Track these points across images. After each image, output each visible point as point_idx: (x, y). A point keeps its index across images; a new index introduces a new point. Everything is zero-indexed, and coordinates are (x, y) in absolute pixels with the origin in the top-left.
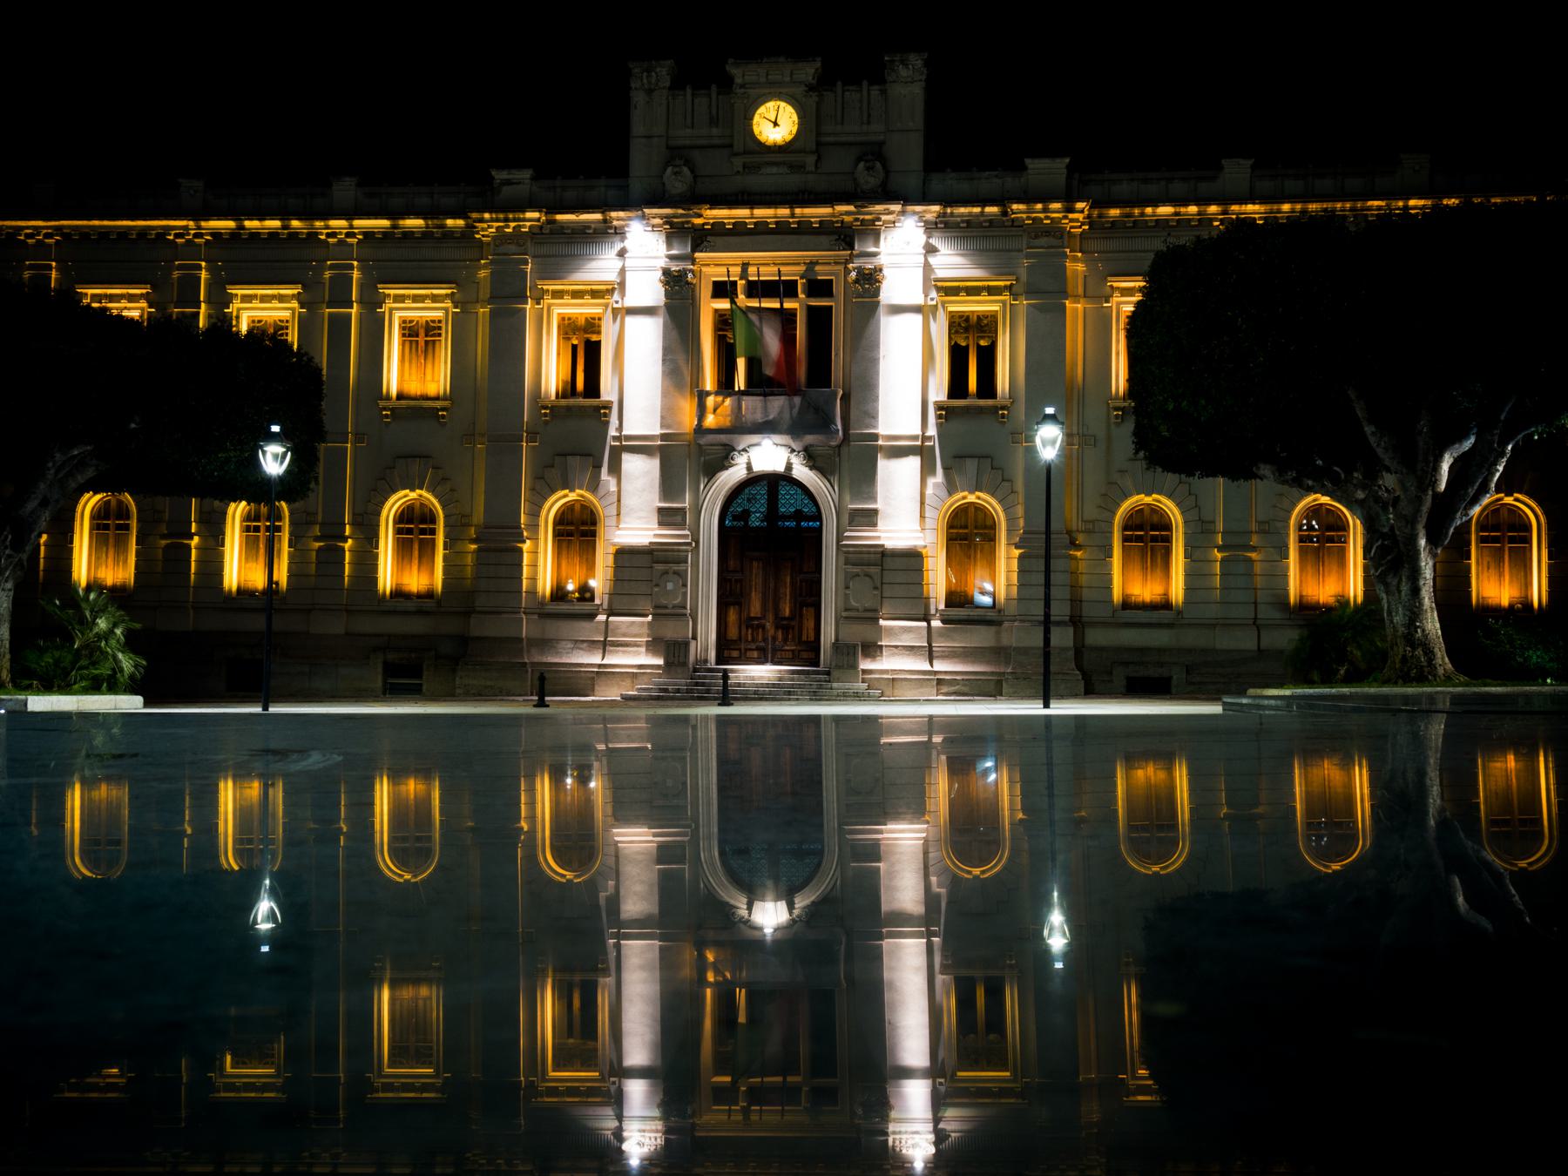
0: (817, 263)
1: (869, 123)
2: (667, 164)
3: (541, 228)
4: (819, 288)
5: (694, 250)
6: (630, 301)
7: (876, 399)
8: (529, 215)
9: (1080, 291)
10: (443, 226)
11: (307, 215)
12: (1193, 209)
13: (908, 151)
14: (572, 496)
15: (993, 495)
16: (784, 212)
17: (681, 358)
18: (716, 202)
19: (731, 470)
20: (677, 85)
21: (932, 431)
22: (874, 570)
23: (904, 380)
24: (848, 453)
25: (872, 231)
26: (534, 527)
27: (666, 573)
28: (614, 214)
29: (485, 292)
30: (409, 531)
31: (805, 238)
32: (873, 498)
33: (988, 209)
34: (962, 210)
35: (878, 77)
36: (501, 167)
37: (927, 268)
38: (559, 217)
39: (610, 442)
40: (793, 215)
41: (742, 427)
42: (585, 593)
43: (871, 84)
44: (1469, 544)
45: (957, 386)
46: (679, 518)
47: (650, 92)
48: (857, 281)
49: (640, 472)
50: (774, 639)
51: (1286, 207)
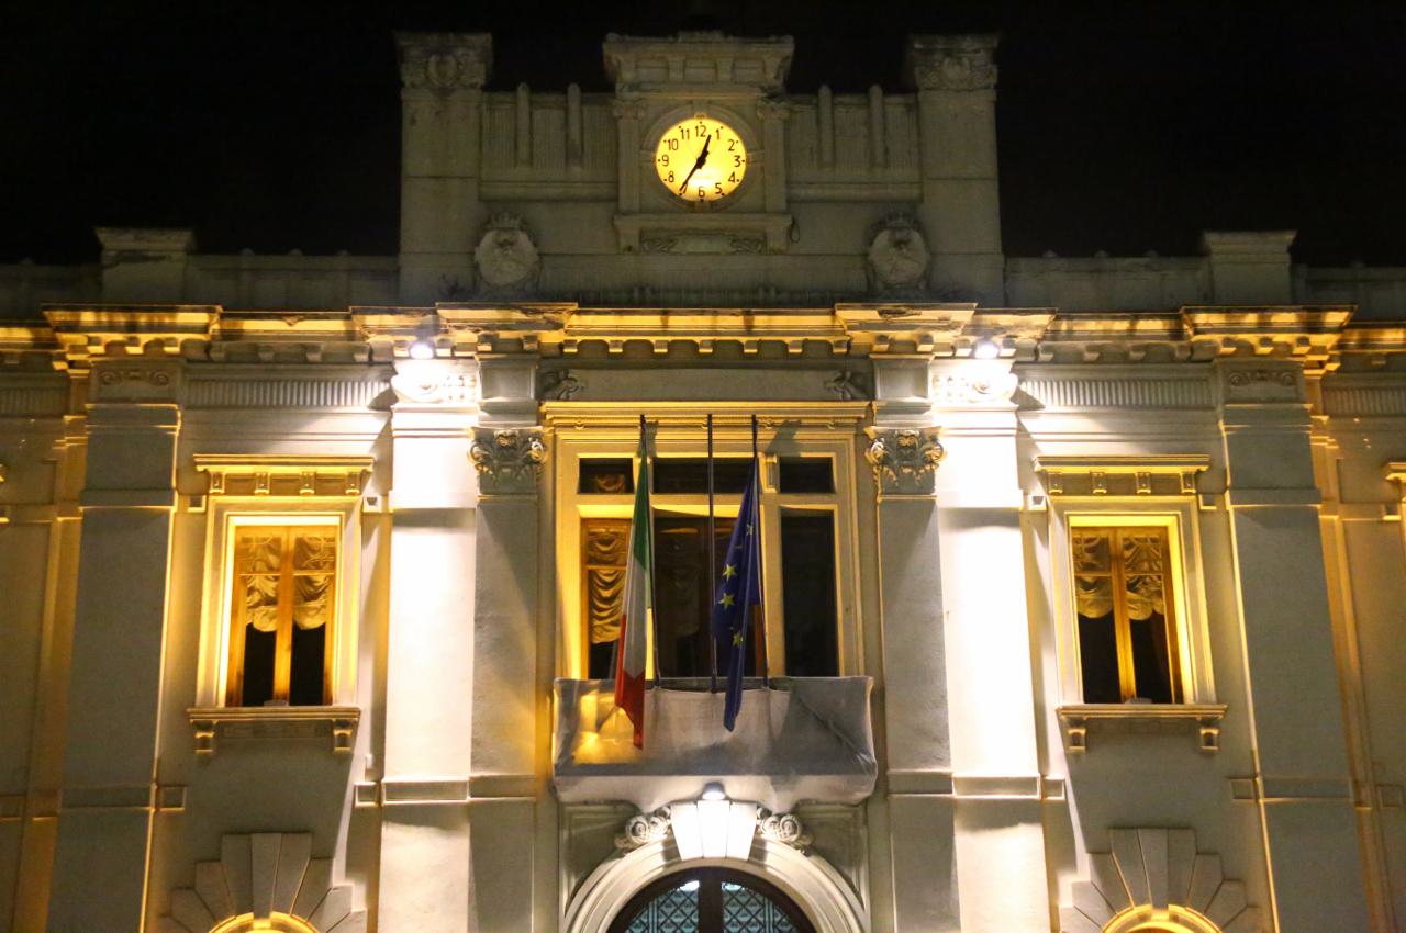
0: (799, 425)
1: (886, 165)
2: (484, 226)
3: (207, 347)
4: (805, 475)
5: (541, 396)
6: (405, 496)
7: (941, 701)
8: (184, 318)
9: (1334, 491)
13: (969, 210)
15: (1205, 911)
16: (731, 321)
17: (521, 620)
18: (591, 301)
19: (630, 858)
20: (500, 82)
21: (1059, 771)
23: (994, 677)
25: (911, 362)
28: (372, 320)
29: (73, 478)
31: (773, 376)
33: (1144, 325)
34: (1092, 326)
35: (899, 83)
36: (121, 222)
38: (250, 325)
39: (352, 801)
40: (749, 330)
45: (1099, 679)
47: (443, 92)
48: (884, 461)
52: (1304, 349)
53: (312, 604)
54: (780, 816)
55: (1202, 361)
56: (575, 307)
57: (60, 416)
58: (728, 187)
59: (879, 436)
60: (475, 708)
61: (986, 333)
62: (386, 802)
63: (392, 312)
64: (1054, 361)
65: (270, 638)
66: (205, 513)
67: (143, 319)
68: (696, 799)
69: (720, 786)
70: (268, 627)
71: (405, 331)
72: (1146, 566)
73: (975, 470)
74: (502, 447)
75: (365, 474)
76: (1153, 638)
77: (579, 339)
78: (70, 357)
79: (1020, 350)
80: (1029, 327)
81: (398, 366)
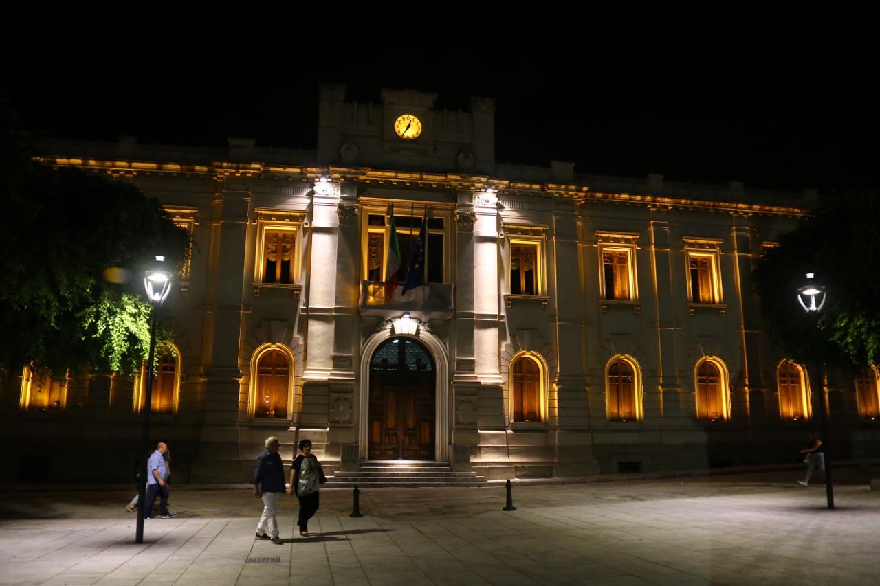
0: (434, 209)
3: (259, 175)
4: (438, 224)
8: (253, 166)
10: (193, 170)
11: (100, 158)
12: (639, 197)
14: (273, 347)
18: (375, 168)
19: (381, 333)
21: (503, 313)
22: (473, 398)
24: (456, 322)
26: (247, 367)
27: (339, 399)
28: (309, 169)
30: (617, 380)
32: (473, 354)
33: (534, 186)
34: (520, 185)
37: (499, 217)
38: (272, 169)
40: (421, 179)
41: (392, 305)
42: (281, 413)
43: (158, 484)
44: (776, 384)
45: (515, 287)
46: (347, 364)
48: (459, 221)
49: (319, 332)
50: (403, 443)
51: (683, 201)
52: (576, 197)
53: (287, 254)
54: (425, 323)
55: (549, 197)
56: (370, 169)
57: (215, 194)
58: (416, 136)
59: (458, 213)
60: (337, 287)
61: (489, 185)
62: (310, 313)
63: (315, 167)
64: (509, 195)
65: (275, 263)
66: (257, 225)
67: (241, 166)
68: (401, 317)
69: (408, 314)
70: (274, 260)
71: (319, 173)
72: (529, 256)
73: (486, 225)
74: (347, 210)
75: (305, 216)
76: (530, 276)
77: (370, 178)
78: (219, 176)
79: (499, 191)
80: (502, 184)
81: (316, 184)
